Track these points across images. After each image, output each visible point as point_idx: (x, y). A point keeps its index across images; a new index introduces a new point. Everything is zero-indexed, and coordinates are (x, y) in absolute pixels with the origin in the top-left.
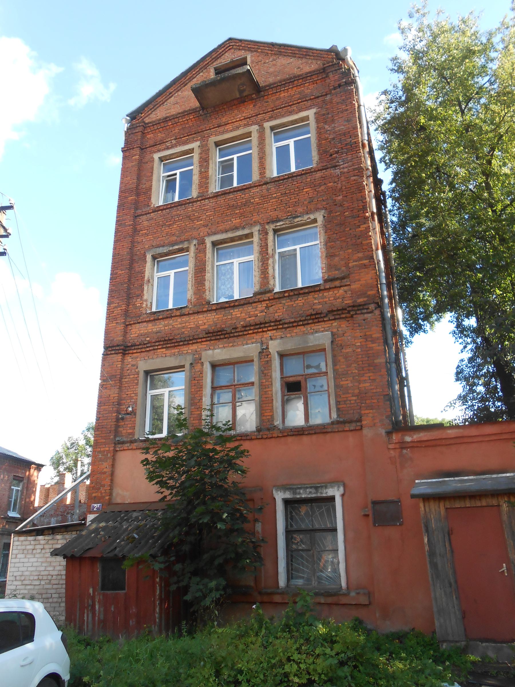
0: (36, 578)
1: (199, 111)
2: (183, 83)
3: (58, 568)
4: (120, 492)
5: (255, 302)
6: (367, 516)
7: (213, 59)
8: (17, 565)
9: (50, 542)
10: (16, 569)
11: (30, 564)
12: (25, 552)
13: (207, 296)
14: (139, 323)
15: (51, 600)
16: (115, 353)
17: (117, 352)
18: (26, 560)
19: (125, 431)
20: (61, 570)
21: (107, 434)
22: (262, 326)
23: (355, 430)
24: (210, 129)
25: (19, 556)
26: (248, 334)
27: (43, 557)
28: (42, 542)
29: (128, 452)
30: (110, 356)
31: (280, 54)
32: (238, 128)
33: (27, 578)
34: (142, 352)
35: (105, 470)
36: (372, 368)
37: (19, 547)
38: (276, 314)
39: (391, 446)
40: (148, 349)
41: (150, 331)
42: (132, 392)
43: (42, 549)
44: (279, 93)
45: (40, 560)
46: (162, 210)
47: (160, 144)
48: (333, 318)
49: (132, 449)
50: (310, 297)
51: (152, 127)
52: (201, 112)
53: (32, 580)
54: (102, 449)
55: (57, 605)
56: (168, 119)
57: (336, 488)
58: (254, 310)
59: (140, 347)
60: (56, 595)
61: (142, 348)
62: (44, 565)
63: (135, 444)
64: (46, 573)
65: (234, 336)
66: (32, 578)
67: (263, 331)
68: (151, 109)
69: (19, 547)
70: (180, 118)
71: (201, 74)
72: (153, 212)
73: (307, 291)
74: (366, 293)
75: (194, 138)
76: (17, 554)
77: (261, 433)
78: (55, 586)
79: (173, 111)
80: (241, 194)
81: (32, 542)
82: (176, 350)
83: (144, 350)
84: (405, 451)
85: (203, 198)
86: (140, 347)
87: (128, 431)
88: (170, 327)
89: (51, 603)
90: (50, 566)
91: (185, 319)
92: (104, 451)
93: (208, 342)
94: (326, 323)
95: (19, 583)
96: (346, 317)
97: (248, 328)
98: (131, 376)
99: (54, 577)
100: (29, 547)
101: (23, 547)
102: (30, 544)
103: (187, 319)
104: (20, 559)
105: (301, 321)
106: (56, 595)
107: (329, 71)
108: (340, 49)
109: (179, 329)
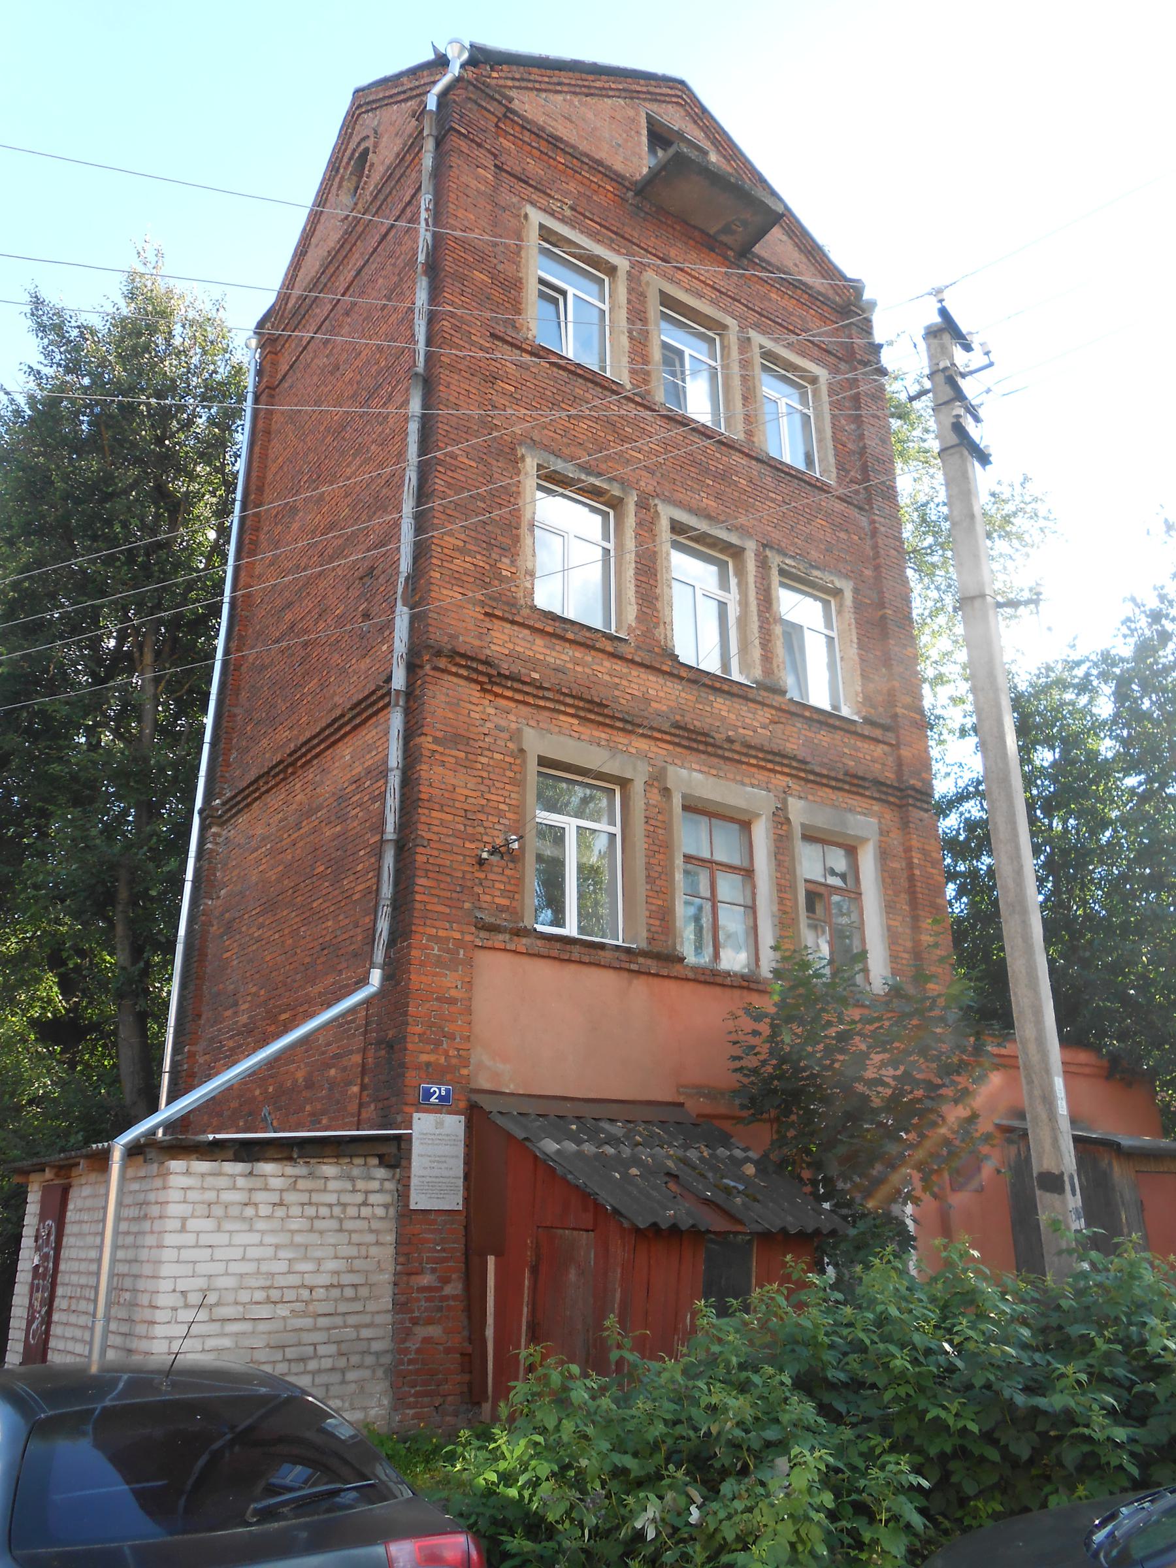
0: (259, 1296)
3: (331, 1265)
4: (486, 1060)
8: (186, 1254)
9: (301, 1184)
10: (186, 1269)
11: (237, 1253)
12: (218, 1211)
14: (513, 622)
15: (312, 1365)
16: (467, 678)
17: (474, 676)
18: (223, 1238)
19: (488, 898)
20: (337, 1273)
21: (454, 895)
25: (192, 1224)
27: (282, 1230)
28: (276, 1183)
29: (499, 955)
30: (450, 678)
32: (700, 296)
33: (230, 1297)
35: (453, 993)
37: (193, 1196)
40: (542, 703)
43: (275, 1204)
45: (269, 1239)
50: (838, 735)
51: (517, 128)
52: (630, 194)
53: (244, 1304)
54: (441, 933)
55: (335, 1378)
60: (332, 1349)
61: (527, 693)
62: (282, 1254)
63: (524, 940)
64: (293, 1280)
66: (244, 1296)
69: (193, 1196)
73: (837, 723)
75: (612, 241)
76: (184, 1220)
78: (322, 1322)
81: (241, 1182)
82: (603, 735)
88: (588, 671)
89: (314, 1373)
90: (305, 1258)
91: (620, 667)
92: (447, 939)
93: (670, 747)
97: (753, 753)
100: (227, 1196)
101: (210, 1196)
102: (234, 1188)
104: (198, 1233)
106: (332, 1349)
108: (867, 296)
109: (606, 685)
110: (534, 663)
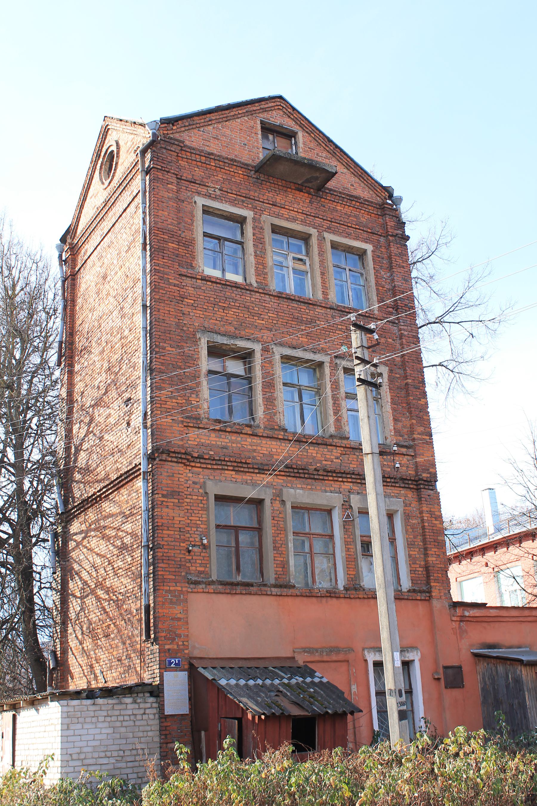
1: (251, 170)
2: (226, 117)
5: (331, 445)
6: (438, 679)
7: (261, 109)
9: (116, 707)
13: (276, 418)
18: (84, 732)
19: (194, 568)
21: (177, 570)
22: (344, 475)
23: (425, 600)
24: (263, 202)
26: (328, 480)
30: (169, 463)
31: (334, 154)
32: (294, 220)
34: (206, 468)
35: (179, 616)
36: (436, 544)
38: (351, 465)
39: (454, 619)
40: (215, 467)
41: (213, 442)
42: (198, 519)
44: (335, 204)
46: (212, 282)
47: (200, 184)
48: (403, 485)
49: (208, 592)
51: (189, 154)
53: (96, 758)
56: (213, 157)
57: (415, 653)
58: (330, 453)
59: (207, 461)
63: (212, 587)
65: (314, 479)
66: (96, 755)
67: (342, 481)
68: (185, 126)
70: (227, 165)
71: (246, 118)
72: (202, 280)
74: (428, 470)
75: (243, 201)
77: (348, 592)
78: (130, 765)
79: (214, 148)
80: (305, 308)
83: (209, 466)
84: (462, 624)
85: (265, 292)
86: (207, 461)
87: (198, 569)
88: (239, 445)
91: (256, 440)
92: (175, 591)
93: (285, 478)
94: (396, 488)
95: (79, 763)
96: (413, 488)
98: (194, 497)
99: (127, 753)
103: (258, 441)
105: (235, 462)
107: (388, 213)
109: (249, 451)
110: (210, 447)
